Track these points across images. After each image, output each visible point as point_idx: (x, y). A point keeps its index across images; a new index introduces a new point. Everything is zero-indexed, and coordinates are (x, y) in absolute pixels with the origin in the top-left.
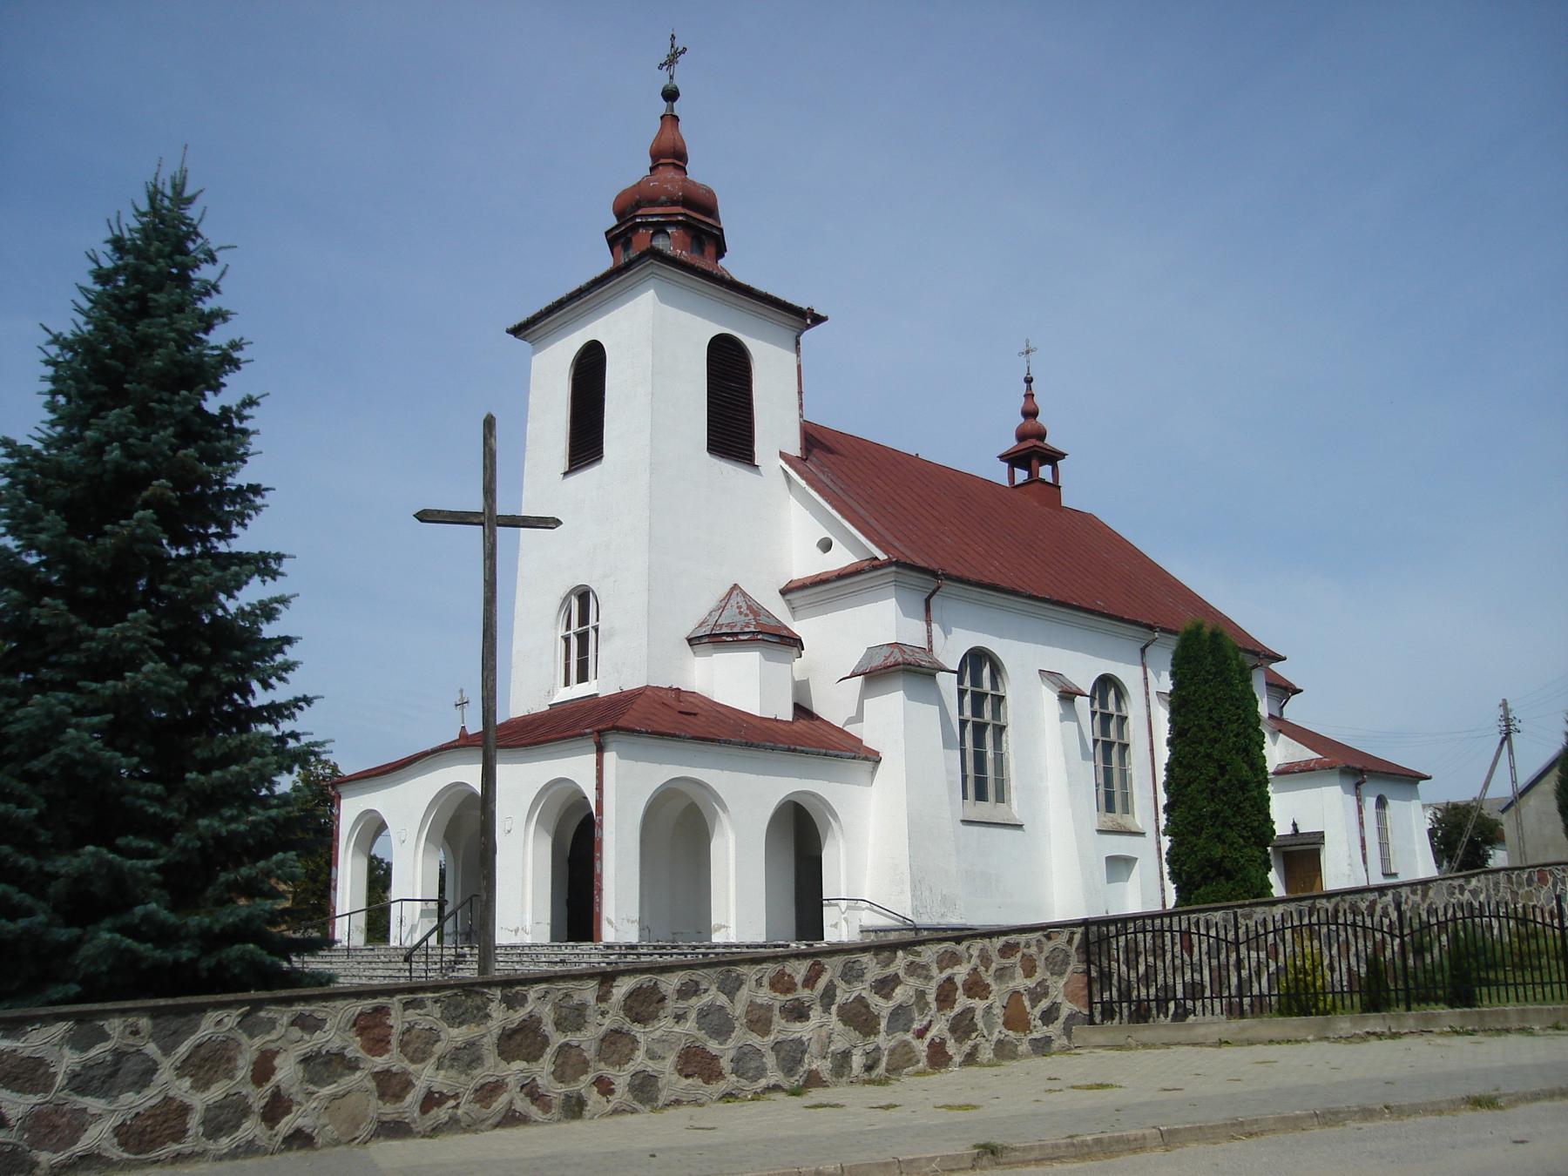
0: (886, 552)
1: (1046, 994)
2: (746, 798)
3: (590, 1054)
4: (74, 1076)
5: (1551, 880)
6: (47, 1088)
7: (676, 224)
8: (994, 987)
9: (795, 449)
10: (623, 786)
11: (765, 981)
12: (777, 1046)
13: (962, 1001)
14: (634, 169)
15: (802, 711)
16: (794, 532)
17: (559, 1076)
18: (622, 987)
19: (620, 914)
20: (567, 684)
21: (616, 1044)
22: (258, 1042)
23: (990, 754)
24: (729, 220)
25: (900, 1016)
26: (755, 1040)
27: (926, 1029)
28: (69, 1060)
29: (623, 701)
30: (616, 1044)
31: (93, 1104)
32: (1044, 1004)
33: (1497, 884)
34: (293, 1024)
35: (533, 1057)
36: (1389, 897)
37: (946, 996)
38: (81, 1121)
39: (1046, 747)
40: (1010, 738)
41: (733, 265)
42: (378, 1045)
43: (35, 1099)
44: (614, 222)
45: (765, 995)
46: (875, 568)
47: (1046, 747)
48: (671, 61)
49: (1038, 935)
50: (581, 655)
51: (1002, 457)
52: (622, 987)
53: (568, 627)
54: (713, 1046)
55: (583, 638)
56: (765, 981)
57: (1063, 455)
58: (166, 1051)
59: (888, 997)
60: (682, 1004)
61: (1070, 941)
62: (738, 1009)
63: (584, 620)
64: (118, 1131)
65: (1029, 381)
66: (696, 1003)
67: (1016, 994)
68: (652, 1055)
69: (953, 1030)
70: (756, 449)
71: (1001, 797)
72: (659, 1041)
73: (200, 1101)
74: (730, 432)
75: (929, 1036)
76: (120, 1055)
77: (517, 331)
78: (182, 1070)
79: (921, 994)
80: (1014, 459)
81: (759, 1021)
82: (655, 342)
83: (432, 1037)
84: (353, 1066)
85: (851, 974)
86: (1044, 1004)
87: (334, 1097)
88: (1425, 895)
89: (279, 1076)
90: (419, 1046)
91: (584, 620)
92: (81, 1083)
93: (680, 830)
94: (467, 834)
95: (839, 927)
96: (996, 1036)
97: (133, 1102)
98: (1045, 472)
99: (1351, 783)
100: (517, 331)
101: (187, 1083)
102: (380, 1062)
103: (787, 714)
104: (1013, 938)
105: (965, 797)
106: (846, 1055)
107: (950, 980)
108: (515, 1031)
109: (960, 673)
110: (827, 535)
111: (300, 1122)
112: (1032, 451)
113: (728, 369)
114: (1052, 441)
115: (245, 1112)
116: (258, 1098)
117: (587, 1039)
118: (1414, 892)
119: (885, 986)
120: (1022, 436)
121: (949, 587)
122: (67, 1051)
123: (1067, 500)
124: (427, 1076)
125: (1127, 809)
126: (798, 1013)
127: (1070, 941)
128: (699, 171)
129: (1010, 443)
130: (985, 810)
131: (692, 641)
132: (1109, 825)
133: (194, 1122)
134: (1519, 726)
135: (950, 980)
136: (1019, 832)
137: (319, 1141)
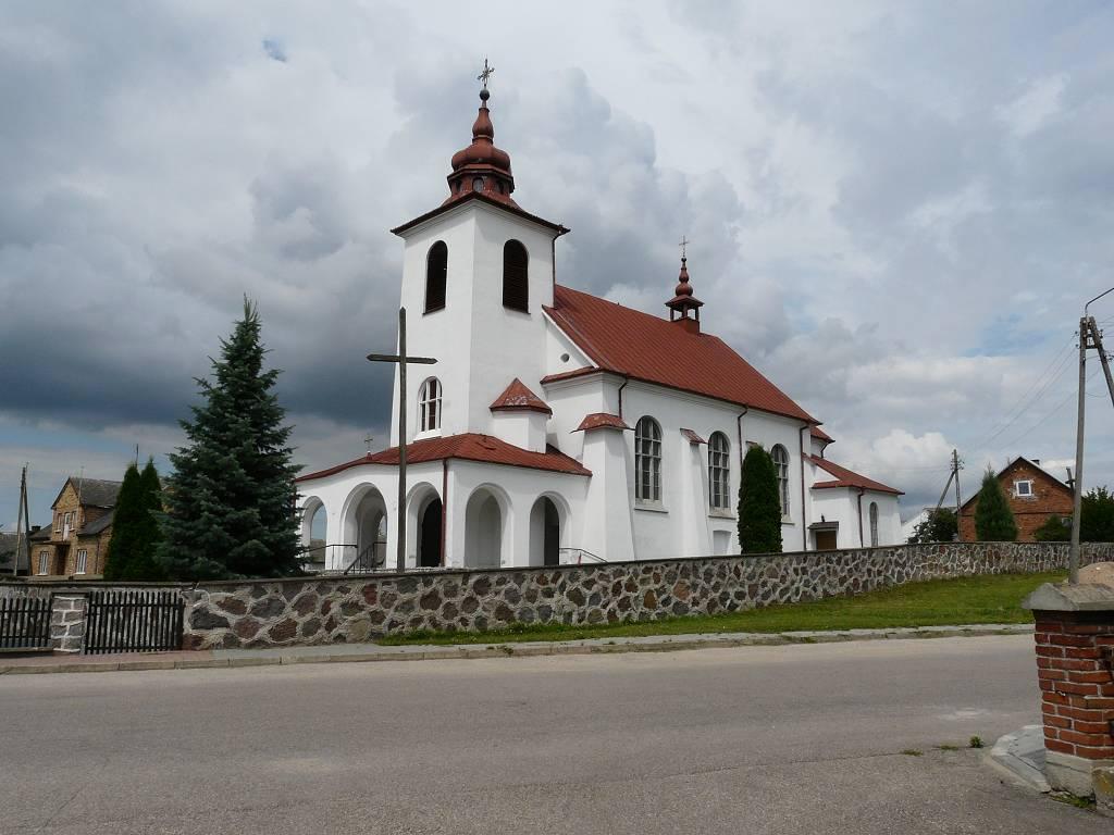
0: (597, 363)
1: (664, 592)
2: (520, 497)
3: (458, 608)
4: (253, 608)
5: (947, 551)
6: (244, 613)
7: (486, 174)
8: (640, 587)
9: (550, 304)
10: (456, 488)
11: (535, 579)
12: (539, 608)
13: (624, 593)
14: (464, 141)
15: (552, 449)
16: (547, 349)
17: (446, 617)
18: (472, 581)
19: (455, 552)
20: (423, 430)
21: (470, 603)
22: (324, 597)
23: (651, 474)
24: (516, 171)
25: (595, 598)
26: (529, 604)
27: (607, 605)
28: (251, 602)
29: (455, 440)
30: (470, 603)
31: (261, 620)
32: (664, 596)
33: (914, 552)
34: (338, 590)
35: (435, 608)
36: (850, 556)
37: (617, 590)
38: (257, 626)
39: (683, 470)
40: (663, 465)
41: (518, 197)
42: (372, 600)
43: (241, 617)
44: (452, 171)
45: (534, 586)
46: (592, 372)
47: (683, 470)
48: (486, 74)
49: (660, 565)
50: (431, 416)
51: (667, 304)
52: (472, 581)
53: (424, 399)
54: (511, 606)
55: (432, 405)
56: (535, 579)
57: (701, 304)
58: (289, 600)
59: (589, 589)
60: (498, 587)
61: (677, 568)
62: (523, 591)
63: (433, 395)
64: (270, 631)
65: (684, 260)
66: (504, 587)
67: (650, 591)
68: (484, 609)
69: (619, 606)
70: (529, 303)
71: (656, 497)
72: (488, 603)
73: (302, 621)
74: (515, 296)
75: (608, 608)
76: (271, 600)
77: (397, 231)
78: (294, 608)
79: (605, 589)
80: (673, 306)
81: (532, 597)
82: (473, 246)
83: (394, 597)
84: (361, 609)
85: (573, 578)
86: (664, 596)
87: (355, 621)
88: (870, 556)
89: (332, 612)
90: (388, 601)
91: (433, 395)
92: (256, 611)
93: (486, 511)
94: (368, 511)
95: (565, 559)
96: (640, 610)
97: (276, 620)
98: (691, 313)
99: (854, 496)
100: (397, 231)
101: (296, 613)
102: (373, 607)
103: (542, 449)
104: (649, 565)
105: (637, 496)
106: (570, 614)
107: (619, 583)
108: (428, 597)
109: (636, 430)
110: (566, 352)
111: (341, 631)
112: (684, 300)
113: (515, 259)
114: (695, 296)
115: (319, 627)
116: (324, 620)
117: (458, 600)
118: (864, 554)
119: (589, 584)
120: (679, 292)
121: (631, 383)
122: (250, 598)
123: (703, 330)
124: (391, 614)
125: (726, 505)
126: (549, 594)
127: (677, 568)
128: (499, 143)
129: (672, 296)
130: (649, 503)
131: (493, 409)
132: (716, 514)
133: (299, 629)
134: (963, 465)
135: (619, 583)
136: (659, 518)
137: (348, 639)
